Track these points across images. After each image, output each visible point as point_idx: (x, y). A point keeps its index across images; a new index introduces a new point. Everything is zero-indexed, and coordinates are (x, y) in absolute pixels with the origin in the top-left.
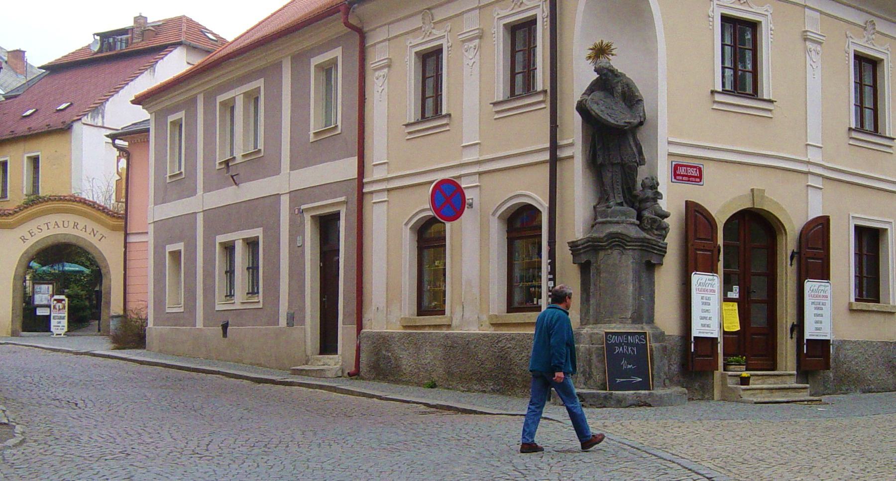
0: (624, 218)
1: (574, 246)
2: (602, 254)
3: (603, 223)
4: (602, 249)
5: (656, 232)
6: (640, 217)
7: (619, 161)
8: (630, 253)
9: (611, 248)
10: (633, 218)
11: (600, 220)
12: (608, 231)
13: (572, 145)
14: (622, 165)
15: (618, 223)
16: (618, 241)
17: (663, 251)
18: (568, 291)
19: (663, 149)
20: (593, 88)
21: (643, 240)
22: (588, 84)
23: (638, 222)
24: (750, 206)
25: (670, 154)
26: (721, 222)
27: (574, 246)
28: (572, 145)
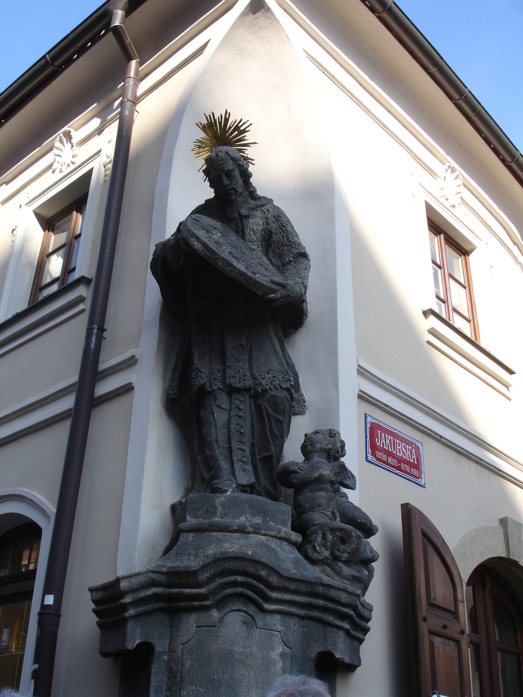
0: (258, 520)
1: (109, 601)
2: (190, 623)
3: (197, 530)
4: (192, 610)
5: (347, 570)
6: (300, 525)
7: (249, 382)
8: (276, 621)
9: (219, 605)
10: (283, 523)
11: (191, 521)
12: (211, 551)
13: (131, 362)
14: (256, 395)
15: (242, 530)
16: (248, 586)
17: (357, 624)
18: (201, 135)
19: (349, 384)
20: (205, 209)
21: (311, 588)
22: (194, 208)
23: (296, 537)
24: (504, 555)
25: (363, 397)
26: (465, 569)
27: (109, 601)
28: (131, 362)
